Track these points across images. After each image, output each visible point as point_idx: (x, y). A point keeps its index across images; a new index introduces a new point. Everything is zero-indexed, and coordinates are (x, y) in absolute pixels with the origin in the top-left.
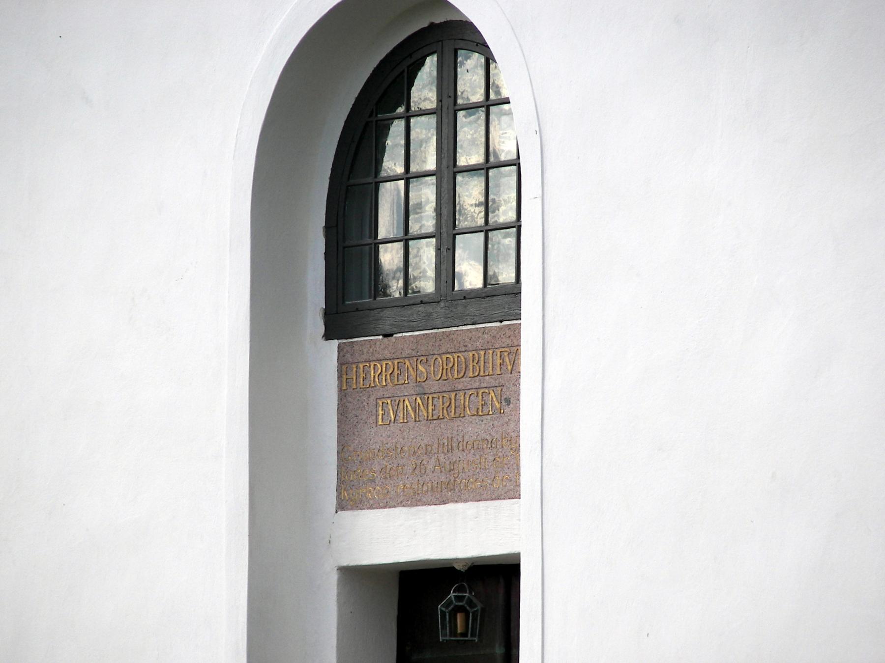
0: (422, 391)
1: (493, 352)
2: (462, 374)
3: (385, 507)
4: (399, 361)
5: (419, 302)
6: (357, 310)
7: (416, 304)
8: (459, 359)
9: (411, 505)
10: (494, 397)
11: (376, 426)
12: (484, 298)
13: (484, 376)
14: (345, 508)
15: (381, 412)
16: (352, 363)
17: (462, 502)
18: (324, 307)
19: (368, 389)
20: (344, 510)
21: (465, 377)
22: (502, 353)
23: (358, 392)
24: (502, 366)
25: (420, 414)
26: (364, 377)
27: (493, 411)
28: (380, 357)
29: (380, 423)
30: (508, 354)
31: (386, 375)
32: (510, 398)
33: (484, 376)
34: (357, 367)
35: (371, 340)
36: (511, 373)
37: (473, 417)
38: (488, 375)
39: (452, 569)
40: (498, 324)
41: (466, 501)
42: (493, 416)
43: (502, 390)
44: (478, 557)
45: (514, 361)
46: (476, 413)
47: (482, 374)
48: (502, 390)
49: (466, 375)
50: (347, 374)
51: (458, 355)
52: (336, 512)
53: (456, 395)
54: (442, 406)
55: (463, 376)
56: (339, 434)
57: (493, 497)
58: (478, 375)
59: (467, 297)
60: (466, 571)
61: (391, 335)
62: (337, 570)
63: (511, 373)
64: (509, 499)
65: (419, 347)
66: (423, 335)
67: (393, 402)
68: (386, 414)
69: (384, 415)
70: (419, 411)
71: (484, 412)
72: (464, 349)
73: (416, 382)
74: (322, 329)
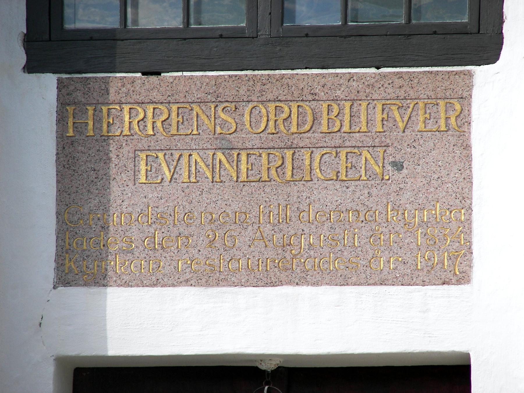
0: (225, 144)
1: (368, 104)
2: (307, 127)
3: (154, 285)
4: (179, 106)
5: (303, 35)
6: (91, 39)
7: (367, 36)
8: (300, 110)
9: (208, 284)
10: (199, 160)
11: (135, 184)
12: (345, 37)
13: (350, 133)
14: (72, 283)
15: (143, 167)
16: (84, 105)
17: (308, 285)
18: (25, 32)
19: (118, 138)
20: (71, 286)
21: (311, 132)
22: (385, 106)
23: (97, 140)
24: (385, 123)
25: (223, 173)
26: (109, 122)
27: (368, 177)
28: (141, 99)
29: (143, 180)
30: (398, 108)
31: (447, 119)
32: (403, 162)
33: (350, 133)
34: (95, 110)
35: (125, 77)
36: (404, 132)
37: (330, 182)
38: (359, 132)
39: (256, 369)
40: (373, 70)
41: (316, 284)
42: (368, 182)
43: (385, 151)
44: (403, 353)
45: (410, 118)
46: (335, 178)
47: (346, 128)
48: (385, 151)
49: (313, 129)
50: (74, 118)
51: (298, 104)
52: (55, 288)
53: (294, 154)
54: (267, 166)
55: (309, 130)
56: (58, 191)
57: (372, 281)
58: (339, 131)
59: (310, 34)
60: (272, 371)
61: (159, 74)
62: (54, 360)
63: (404, 132)
64: (402, 285)
65: (221, 90)
66: (230, 76)
67: (167, 157)
68: (154, 170)
69: (151, 171)
70: (220, 170)
71: (349, 176)
72: (310, 97)
73: (214, 134)
74: (22, 58)
